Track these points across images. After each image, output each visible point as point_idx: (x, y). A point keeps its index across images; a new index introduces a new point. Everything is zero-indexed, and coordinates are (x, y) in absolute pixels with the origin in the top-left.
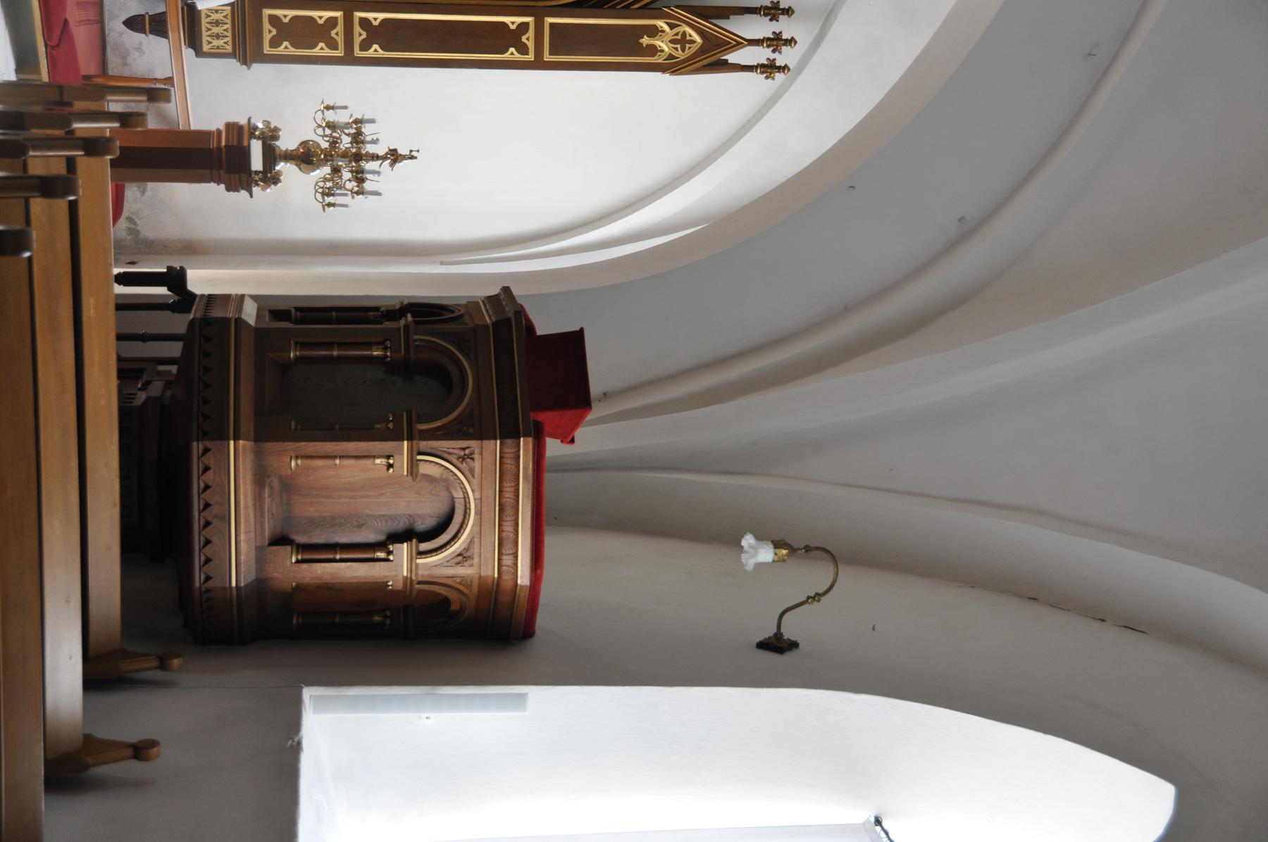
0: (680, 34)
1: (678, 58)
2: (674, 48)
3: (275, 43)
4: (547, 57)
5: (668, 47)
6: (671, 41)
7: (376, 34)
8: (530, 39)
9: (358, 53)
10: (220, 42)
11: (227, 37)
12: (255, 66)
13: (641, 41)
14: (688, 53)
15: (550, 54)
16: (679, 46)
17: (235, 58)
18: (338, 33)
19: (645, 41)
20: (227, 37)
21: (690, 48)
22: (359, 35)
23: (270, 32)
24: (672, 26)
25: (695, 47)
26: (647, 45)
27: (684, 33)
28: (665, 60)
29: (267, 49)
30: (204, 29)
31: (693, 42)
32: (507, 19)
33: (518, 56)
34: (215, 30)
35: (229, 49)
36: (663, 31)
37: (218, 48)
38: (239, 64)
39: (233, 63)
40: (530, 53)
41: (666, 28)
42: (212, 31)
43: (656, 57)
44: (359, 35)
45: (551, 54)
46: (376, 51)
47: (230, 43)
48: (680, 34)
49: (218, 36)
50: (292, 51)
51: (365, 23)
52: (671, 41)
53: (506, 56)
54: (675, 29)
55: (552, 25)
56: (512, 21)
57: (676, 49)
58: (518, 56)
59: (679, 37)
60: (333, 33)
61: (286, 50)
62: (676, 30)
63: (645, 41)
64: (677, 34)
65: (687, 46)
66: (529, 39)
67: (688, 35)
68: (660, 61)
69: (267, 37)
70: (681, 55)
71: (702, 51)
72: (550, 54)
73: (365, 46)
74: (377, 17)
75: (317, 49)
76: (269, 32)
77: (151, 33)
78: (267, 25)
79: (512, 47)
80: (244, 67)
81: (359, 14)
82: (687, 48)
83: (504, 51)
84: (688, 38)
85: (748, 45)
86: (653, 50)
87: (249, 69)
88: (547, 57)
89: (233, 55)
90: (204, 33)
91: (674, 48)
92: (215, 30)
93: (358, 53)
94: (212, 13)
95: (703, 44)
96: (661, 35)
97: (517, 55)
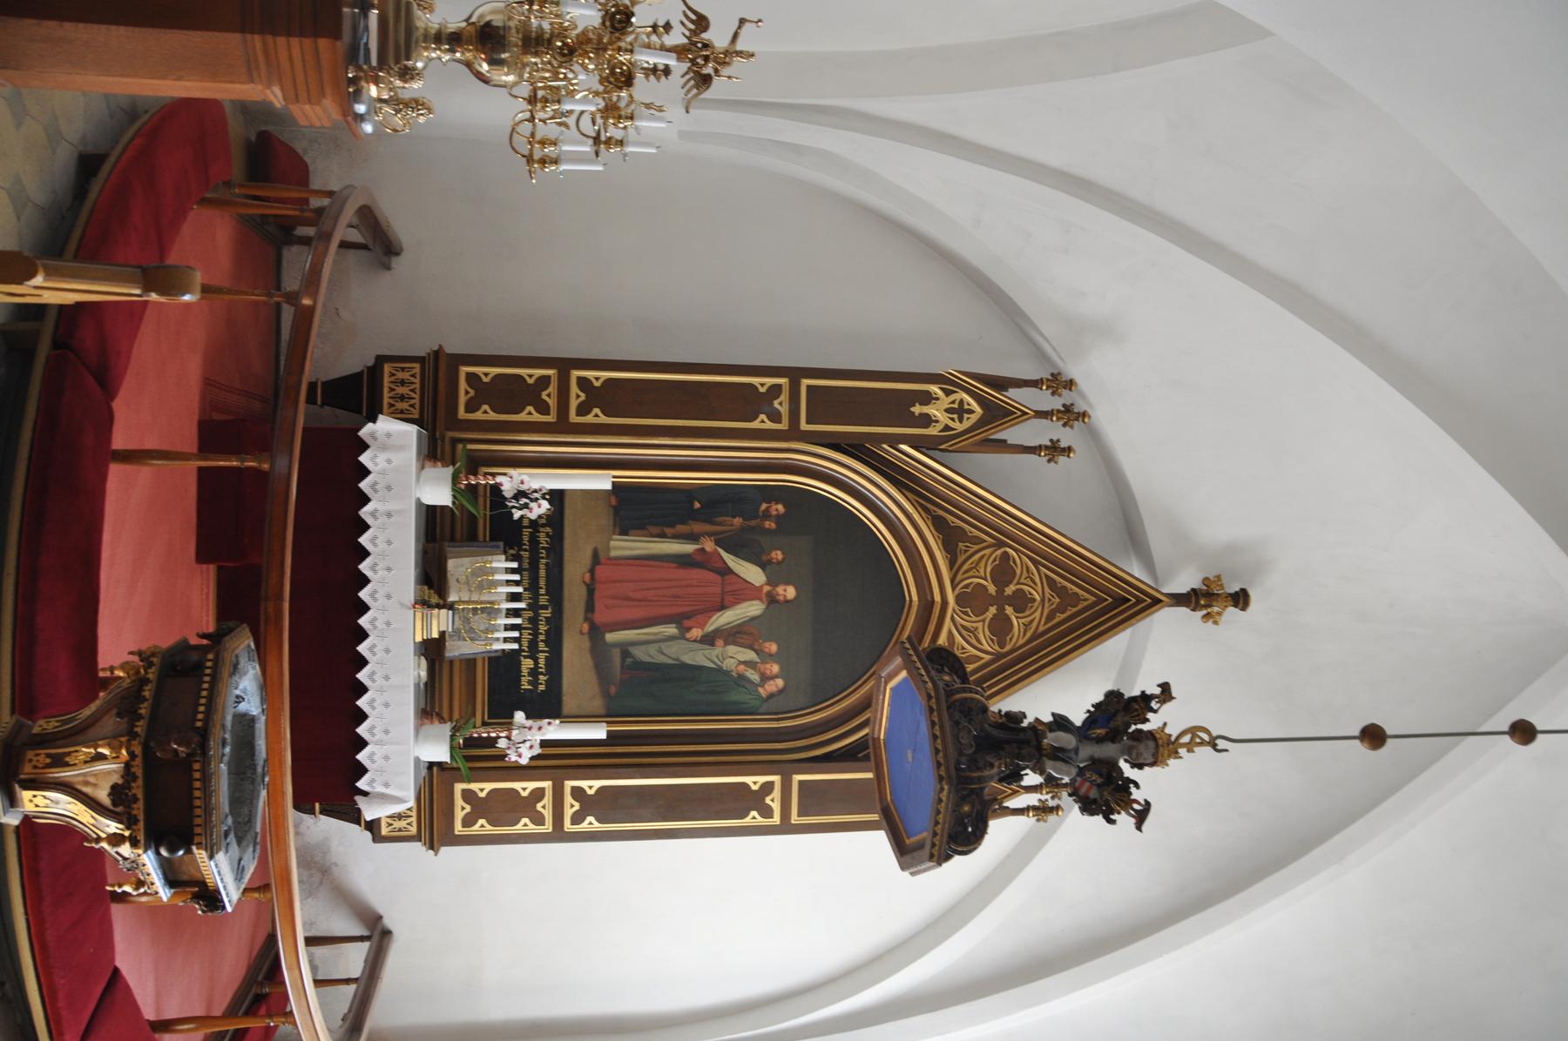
0: (951, 416)
1: (955, 429)
2: (950, 418)
3: (468, 821)
4: (795, 819)
5: (942, 415)
6: (947, 411)
7: (589, 804)
8: (775, 800)
9: (574, 418)
10: (403, 824)
11: (411, 816)
12: (444, 850)
13: (912, 409)
14: (966, 424)
15: (799, 816)
16: (955, 416)
17: (421, 841)
18: (545, 807)
19: (917, 409)
20: (411, 816)
21: (968, 418)
22: (571, 806)
23: (463, 808)
24: (948, 393)
25: (974, 418)
26: (921, 414)
27: (962, 401)
28: (940, 432)
29: (459, 828)
30: (386, 390)
31: (971, 412)
32: (748, 780)
33: (760, 821)
34: (401, 390)
35: (413, 830)
36: (937, 399)
37: (400, 830)
38: (424, 848)
39: (417, 847)
40: (775, 816)
41: (940, 393)
42: (396, 377)
43: (930, 429)
44: (571, 806)
45: (808, 422)
46: (591, 823)
47: (415, 824)
48: (957, 402)
49: (403, 383)
50: (489, 829)
51: (578, 793)
52: (947, 411)
53: (747, 821)
54: (951, 396)
55: (809, 387)
56: (754, 781)
57: (953, 419)
58: (760, 821)
59: (956, 406)
60: (539, 806)
61: (482, 829)
62: (952, 398)
63: (917, 409)
64: (953, 402)
65: (966, 416)
66: (774, 801)
67: (965, 404)
68: (935, 433)
69: (459, 815)
70: (959, 427)
71: (981, 423)
72: (799, 816)
73: (577, 818)
74: (591, 786)
75: (519, 826)
76: (461, 809)
77: (321, 813)
78: (459, 801)
79: (753, 810)
80: (431, 852)
81: (569, 784)
82: (965, 418)
83: (744, 815)
84: (966, 407)
85: (1035, 417)
86: (927, 420)
87: (436, 855)
88: (804, 426)
89: (417, 838)
90: (386, 394)
91: (950, 418)
92: (401, 390)
93: (568, 826)
94: (407, 410)
95: (983, 415)
96: (935, 426)
97: (760, 819)
